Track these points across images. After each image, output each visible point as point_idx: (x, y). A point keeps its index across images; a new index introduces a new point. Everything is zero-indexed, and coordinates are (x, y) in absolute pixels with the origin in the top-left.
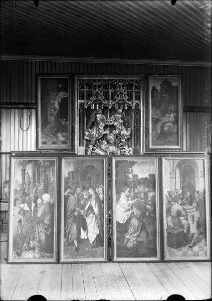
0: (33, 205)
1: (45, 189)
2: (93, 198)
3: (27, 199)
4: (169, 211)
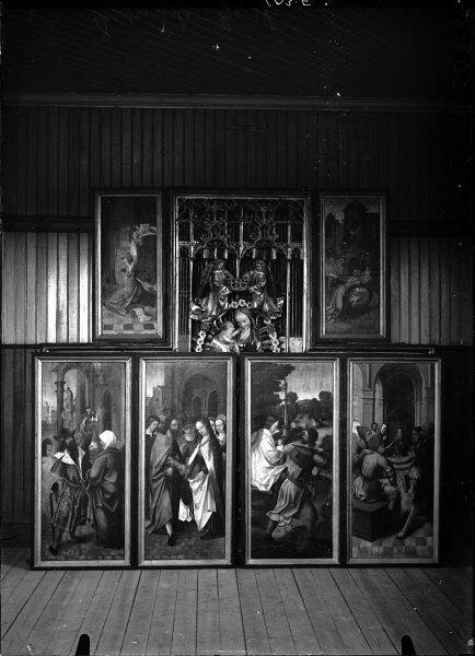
0: (82, 453)
4: (358, 466)
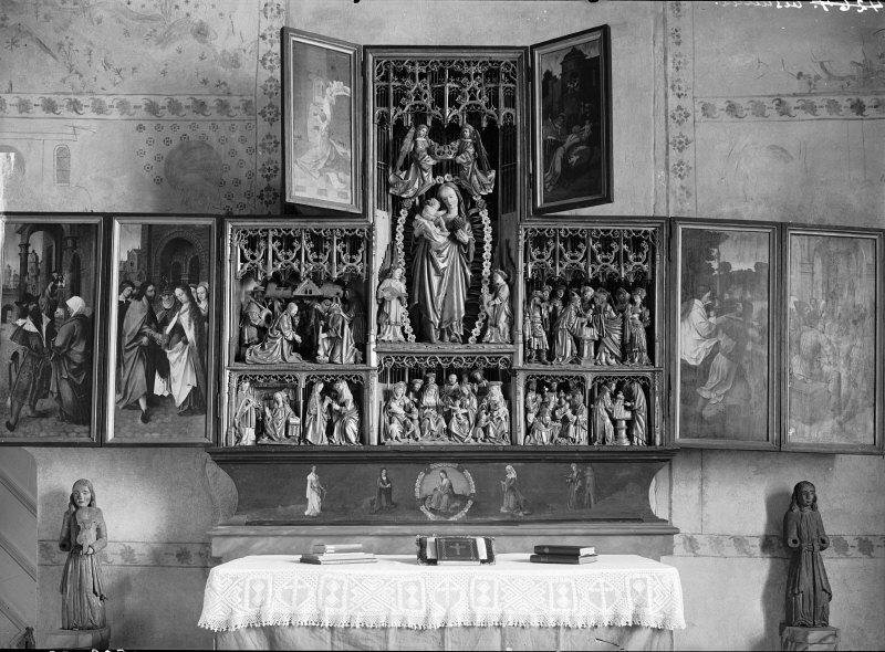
0: (46, 320)
1: (72, 287)
2: (183, 309)
3: (31, 307)
